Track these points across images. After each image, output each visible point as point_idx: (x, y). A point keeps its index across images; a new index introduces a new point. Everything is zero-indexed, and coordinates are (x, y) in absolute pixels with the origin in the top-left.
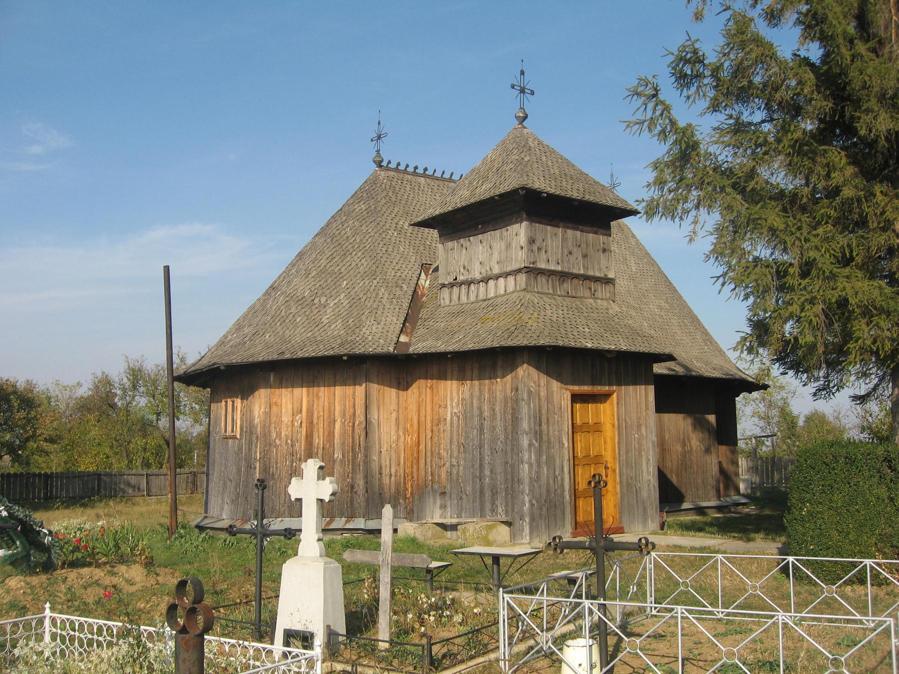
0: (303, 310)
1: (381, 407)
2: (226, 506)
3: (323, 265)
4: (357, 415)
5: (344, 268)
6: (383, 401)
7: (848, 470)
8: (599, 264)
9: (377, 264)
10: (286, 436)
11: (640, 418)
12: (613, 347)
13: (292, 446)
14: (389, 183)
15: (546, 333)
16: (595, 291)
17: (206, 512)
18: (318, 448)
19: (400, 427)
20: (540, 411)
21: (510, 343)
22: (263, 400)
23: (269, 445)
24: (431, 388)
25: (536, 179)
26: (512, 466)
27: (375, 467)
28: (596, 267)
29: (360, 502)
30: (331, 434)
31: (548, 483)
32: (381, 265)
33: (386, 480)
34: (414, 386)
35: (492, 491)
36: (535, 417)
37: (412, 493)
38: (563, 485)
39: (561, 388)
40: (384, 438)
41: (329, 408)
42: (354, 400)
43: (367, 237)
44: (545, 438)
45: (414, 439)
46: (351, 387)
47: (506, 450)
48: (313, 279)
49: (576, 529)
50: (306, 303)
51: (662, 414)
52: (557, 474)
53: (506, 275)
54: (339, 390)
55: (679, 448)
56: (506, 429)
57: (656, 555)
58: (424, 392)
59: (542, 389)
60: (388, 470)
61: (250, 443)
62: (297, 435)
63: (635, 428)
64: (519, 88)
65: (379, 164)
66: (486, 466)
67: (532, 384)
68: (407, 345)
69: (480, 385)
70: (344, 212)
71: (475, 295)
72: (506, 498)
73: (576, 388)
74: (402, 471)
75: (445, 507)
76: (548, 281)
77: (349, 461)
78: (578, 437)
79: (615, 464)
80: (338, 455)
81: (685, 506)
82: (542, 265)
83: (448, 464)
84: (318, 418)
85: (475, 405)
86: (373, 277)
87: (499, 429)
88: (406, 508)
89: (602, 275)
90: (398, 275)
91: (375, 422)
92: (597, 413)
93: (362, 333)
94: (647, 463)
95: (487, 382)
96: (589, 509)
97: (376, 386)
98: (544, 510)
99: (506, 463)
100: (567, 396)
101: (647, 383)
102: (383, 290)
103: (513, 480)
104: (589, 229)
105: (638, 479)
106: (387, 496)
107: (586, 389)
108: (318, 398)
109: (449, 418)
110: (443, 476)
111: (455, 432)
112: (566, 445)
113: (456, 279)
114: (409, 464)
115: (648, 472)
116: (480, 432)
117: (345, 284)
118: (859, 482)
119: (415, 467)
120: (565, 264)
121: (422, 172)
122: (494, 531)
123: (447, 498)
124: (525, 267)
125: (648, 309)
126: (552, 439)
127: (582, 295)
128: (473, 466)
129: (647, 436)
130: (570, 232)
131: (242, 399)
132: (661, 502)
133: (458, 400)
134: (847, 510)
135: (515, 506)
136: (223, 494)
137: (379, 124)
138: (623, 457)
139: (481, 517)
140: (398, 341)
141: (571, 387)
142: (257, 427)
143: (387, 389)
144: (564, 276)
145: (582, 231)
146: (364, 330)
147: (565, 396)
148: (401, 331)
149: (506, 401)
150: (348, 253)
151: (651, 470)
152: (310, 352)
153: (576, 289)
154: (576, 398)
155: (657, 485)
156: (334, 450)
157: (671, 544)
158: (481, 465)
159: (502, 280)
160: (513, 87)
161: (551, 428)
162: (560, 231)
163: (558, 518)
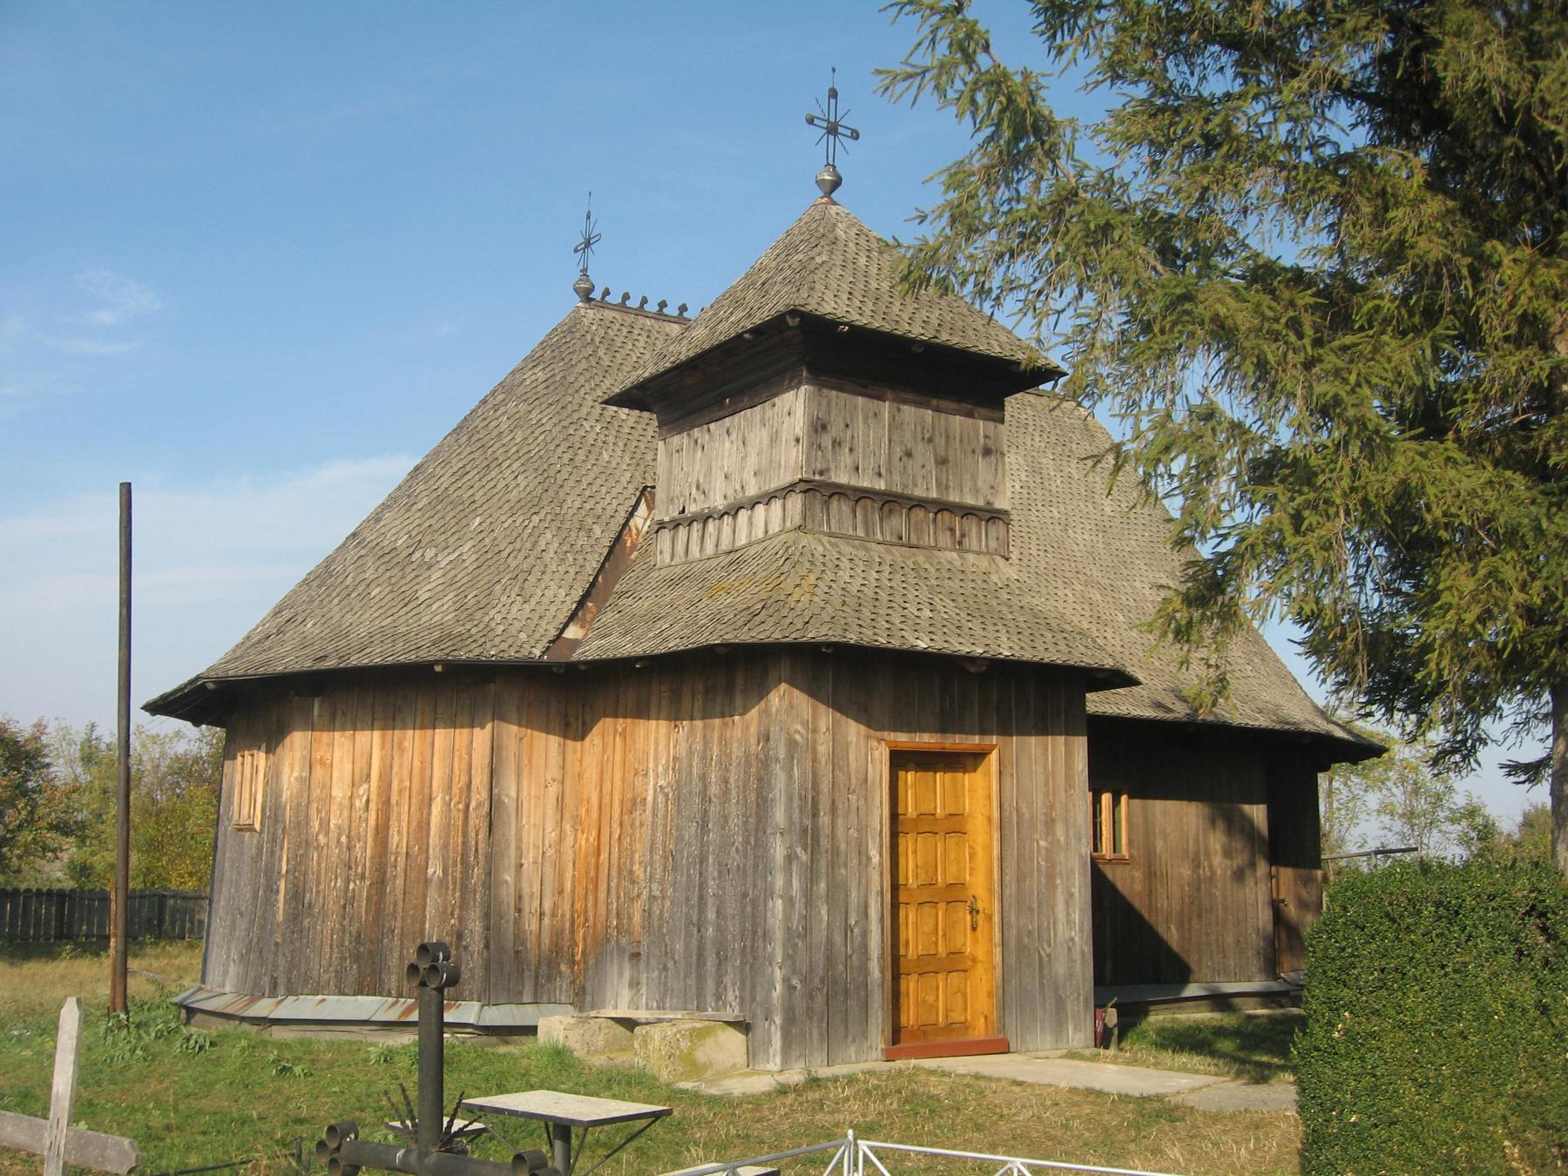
0: (388, 574)
1: (525, 773)
2: (232, 968)
3: (444, 486)
4: (474, 788)
5: (481, 492)
6: (530, 761)
7: (1442, 935)
8: (974, 478)
9: (546, 486)
10: (339, 827)
11: (1052, 807)
12: (1007, 653)
13: (349, 848)
14: (602, 332)
15: (825, 617)
16: (963, 535)
17: (203, 981)
18: (397, 854)
19: (567, 815)
20: (815, 785)
21: (745, 636)
22: (298, 755)
23: (305, 844)
24: (623, 734)
25: (829, 296)
26: (754, 903)
27: (507, 895)
28: (968, 486)
29: (473, 968)
30: (424, 826)
31: (830, 939)
32: (555, 488)
33: (531, 925)
34: (596, 730)
35: (718, 953)
36: (802, 798)
37: (583, 953)
38: (865, 948)
39: (868, 737)
40: (530, 838)
41: (422, 770)
42: (470, 756)
43: (537, 433)
44: (824, 842)
45: (591, 839)
46: (466, 731)
47: (745, 866)
48: (419, 514)
49: (894, 1043)
50: (395, 561)
51: (1150, 802)
52: (852, 921)
53: (768, 498)
54: (441, 736)
55: (1186, 872)
56: (745, 823)
57: (871, 1148)
58: (611, 743)
59: (821, 738)
60: (536, 903)
61: (274, 840)
62: (359, 826)
63: (1041, 827)
64: (825, 124)
65: (586, 296)
66: (710, 901)
67: (799, 727)
68: (576, 643)
69: (705, 728)
70: (507, 388)
71: (714, 542)
72: (742, 971)
73: (903, 739)
74: (567, 906)
75: (638, 984)
76: (854, 512)
77: (454, 883)
78: (907, 844)
79: (991, 903)
80: (435, 870)
81: (1192, 990)
82: (842, 478)
83: (645, 895)
84: (400, 792)
85: (695, 770)
86: (533, 511)
87: (735, 823)
88: (573, 982)
89: (981, 503)
90: (587, 506)
91: (511, 806)
92: (957, 795)
93: (487, 619)
94: (1067, 903)
95: (717, 722)
96: (931, 999)
97: (514, 729)
98: (820, 999)
99: (745, 895)
100: (881, 754)
101: (1070, 731)
102: (549, 535)
103: (756, 931)
104: (954, 405)
105: (1045, 937)
106: (532, 956)
107: (927, 740)
108: (402, 751)
109: (650, 799)
110: (637, 918)
111: (660, 828)
112: (875, 860)
113: (683, 511)
114: (580, 891)
115: (1069, 921)
116: (702, 828)
117: (477, 522)
118: (1466, 964)
119: (591, 897)
120: (896, 477)
121: (676, 313)
122: (709, 1042)
123: (642, 965)
124: (801, 480)
125: (1129, 590)
126: (843, 846)
127: (932, 544)
128: (688, 899)
129: (1067, 844)
130: (909, 412)
131: (267, 752)
132: (1099, 980)
133: (668, 761)
134: (1436, 1031)
135: (758, 989)
136: (229, 942)
137: (588, 217)
138: (1011, 890)
139: (698, 1009)
140: (559, 636)
141: (887, 735)
142: (285, 808)
143: (539, 738)
144: (890, 502)
145: (937, 410)
146: (492, 613)
147: (877, 753)
148: (572, 617)
149: (748, 764)
150: (495, 463)
151: (1076, 917)
152: (376, 655)
153: (919, 531)
154: (900, 760)
155: (1088, 949)
156: (427, 859)
157: (1081, 1086)
158: (701, 897)
159: (760, 509)
160: (811, 121)
161: (840, 822)
162: (886, 408)
163: (850, 1017)
